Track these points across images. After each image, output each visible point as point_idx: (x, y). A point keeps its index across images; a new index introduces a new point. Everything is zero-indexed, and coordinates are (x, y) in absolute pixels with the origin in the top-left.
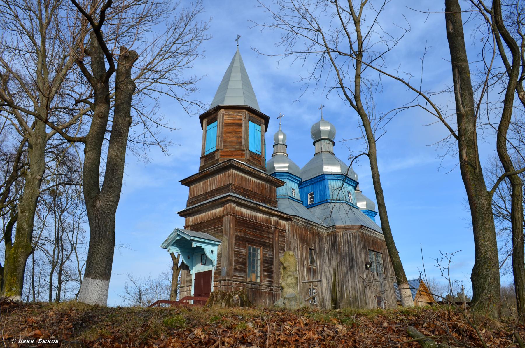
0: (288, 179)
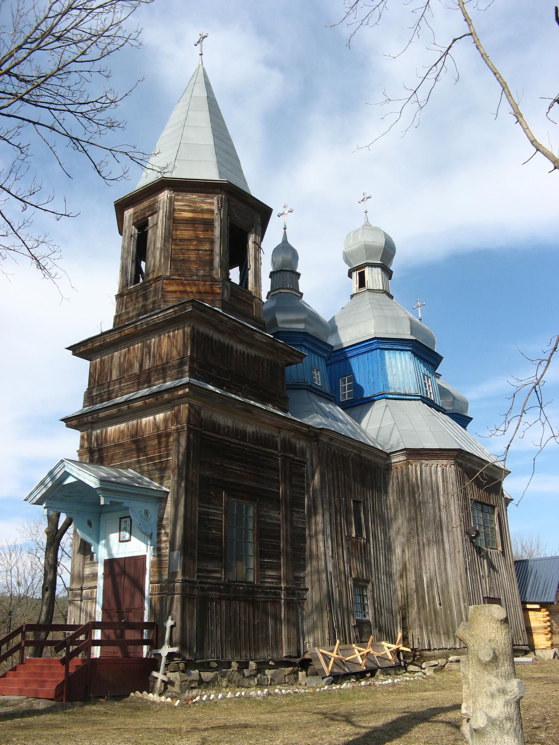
0: (306, 347)
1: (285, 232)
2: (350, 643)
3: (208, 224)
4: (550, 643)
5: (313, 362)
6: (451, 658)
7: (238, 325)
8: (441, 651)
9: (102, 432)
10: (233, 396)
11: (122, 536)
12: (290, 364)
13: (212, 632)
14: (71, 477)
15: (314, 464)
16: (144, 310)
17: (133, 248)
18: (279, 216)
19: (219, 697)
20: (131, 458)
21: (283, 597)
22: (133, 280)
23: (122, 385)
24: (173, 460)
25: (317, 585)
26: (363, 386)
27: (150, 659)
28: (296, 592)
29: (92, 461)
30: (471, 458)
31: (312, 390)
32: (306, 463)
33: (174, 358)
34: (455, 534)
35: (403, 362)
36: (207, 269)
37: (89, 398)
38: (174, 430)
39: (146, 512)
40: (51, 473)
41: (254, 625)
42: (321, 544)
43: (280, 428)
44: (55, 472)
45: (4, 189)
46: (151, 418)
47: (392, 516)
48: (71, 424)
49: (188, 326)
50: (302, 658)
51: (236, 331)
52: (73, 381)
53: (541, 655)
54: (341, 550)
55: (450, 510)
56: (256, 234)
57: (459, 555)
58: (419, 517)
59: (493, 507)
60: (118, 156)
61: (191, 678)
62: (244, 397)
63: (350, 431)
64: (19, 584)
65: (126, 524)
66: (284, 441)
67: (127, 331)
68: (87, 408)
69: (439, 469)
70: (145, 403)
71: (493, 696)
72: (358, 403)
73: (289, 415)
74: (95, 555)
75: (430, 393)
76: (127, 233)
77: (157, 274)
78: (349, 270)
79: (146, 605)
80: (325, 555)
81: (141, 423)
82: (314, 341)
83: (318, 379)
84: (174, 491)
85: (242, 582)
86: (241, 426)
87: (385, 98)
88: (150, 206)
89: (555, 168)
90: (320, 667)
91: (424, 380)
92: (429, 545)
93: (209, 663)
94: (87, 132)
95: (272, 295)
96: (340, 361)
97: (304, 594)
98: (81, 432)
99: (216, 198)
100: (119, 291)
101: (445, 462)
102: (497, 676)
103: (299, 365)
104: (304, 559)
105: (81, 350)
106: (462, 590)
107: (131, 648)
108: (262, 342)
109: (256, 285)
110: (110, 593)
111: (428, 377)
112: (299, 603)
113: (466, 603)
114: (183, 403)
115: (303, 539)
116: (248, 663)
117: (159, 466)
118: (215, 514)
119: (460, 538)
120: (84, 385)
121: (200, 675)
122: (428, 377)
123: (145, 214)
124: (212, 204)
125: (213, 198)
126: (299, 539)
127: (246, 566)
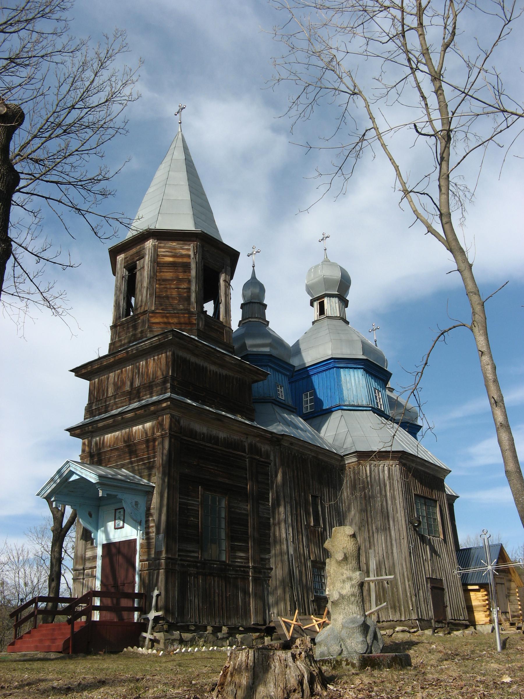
0: (271, 367)
1: (254, 270)
2: (309, 614)
3: (186, 267)
4: (489, 619)
5: (277, 379)
6: (398, 629)
7: (210, 349)
8: (389, 623)
9: (100, 440)
10: (208, 408)
11: (116, 524)
12: (257, 381)
13: (191, 601)
14: (75, 475)
15: (277, 464)
16: (134, 338)
17: (124, 287)
19: (195, 650)
20: (125, 460)
21: (250, 574)
22: (125, 313)
23: (117, 400)
24: (158, 460)
25: (280, 565)
26: (322, 399)
27: (141, 623)
28: (263, 571)
29: (92, 463)
30: (414, 458)
31: (277, 403)
32: (270, 464)
33: (158, 377)
34: (400, 524)
35: (357, 378)
36: (186, 303)
37: (89, 411)
38: (158, 436)
39: (137, 503)
40: (59, 472)
41: (226, 597)
42: (283, 531)
43: (247, 434)
44: (62, 471)
45: (23, 247)
46: (140, 427)
47: (346, 509)
48: (74, 433)
49: (170, 351)
50: (267, 625)
51: (209, 355)
52: (74, 399)
53: (481, 630)
54: (301, 536)
55: (395, 504)
56: (226, 274)
57: (404, 542)
58: (369, 508)
59: (436, 501)
60: (110, 221)
61: (173, 637)
62: (216, 409)
63: (309, 437)
64: (26, 584)
65: (120, 514)
66: (250, 445)
67: (120, 355)
68: (88, 420)
69: (386, 468)
70: (136, 414)
71: (344, 581)
72: (318, 414)
73: (255, 424)
74: (95, 540)
75: (381, 405)
76: (119, 274)
77: (144, 308)
78: (311, 300)
79: (137, 579)
80: (287, 540)
81: (132, 431)
82: (280, 360)
83: (282, 394)
84: (158, 486)
85: (216, 561)
86: (214, 432)
87: (318, 174)
88: (137, 252)
89: (428, 232)
90: (282, 633)
91: (375, 393)
92: (377, 532)
93: (188, 626)
94: (86, 202)
95: (243, 324)
96: (303, 379)
97: (269, 573)
98: (83, 439)
99: (192, 245)
100: (113, 322)
101: (391, 462)
102: (347, 570)
103: (266, 382)
104: (269, 544)
105: (80, 372)
106: (407, 571)
107: (125, 614)
108: (232, 363)
109: (226, 316)
110: (108, 570)
111: (379, 391)
112: (265, 581)
113: (410, 582)
114: (166, 414)
115: (268, 526)
116: (221, 627)
117: (147, 465)
118: (193, 505)
119: (404, 526)
120: (85, 401)
121: (181, 635)
122: (379, 391)
123: (133, 259)
124: (189, 250)
125: (190, 245)
126: (265, 528)
127: (219, 548)
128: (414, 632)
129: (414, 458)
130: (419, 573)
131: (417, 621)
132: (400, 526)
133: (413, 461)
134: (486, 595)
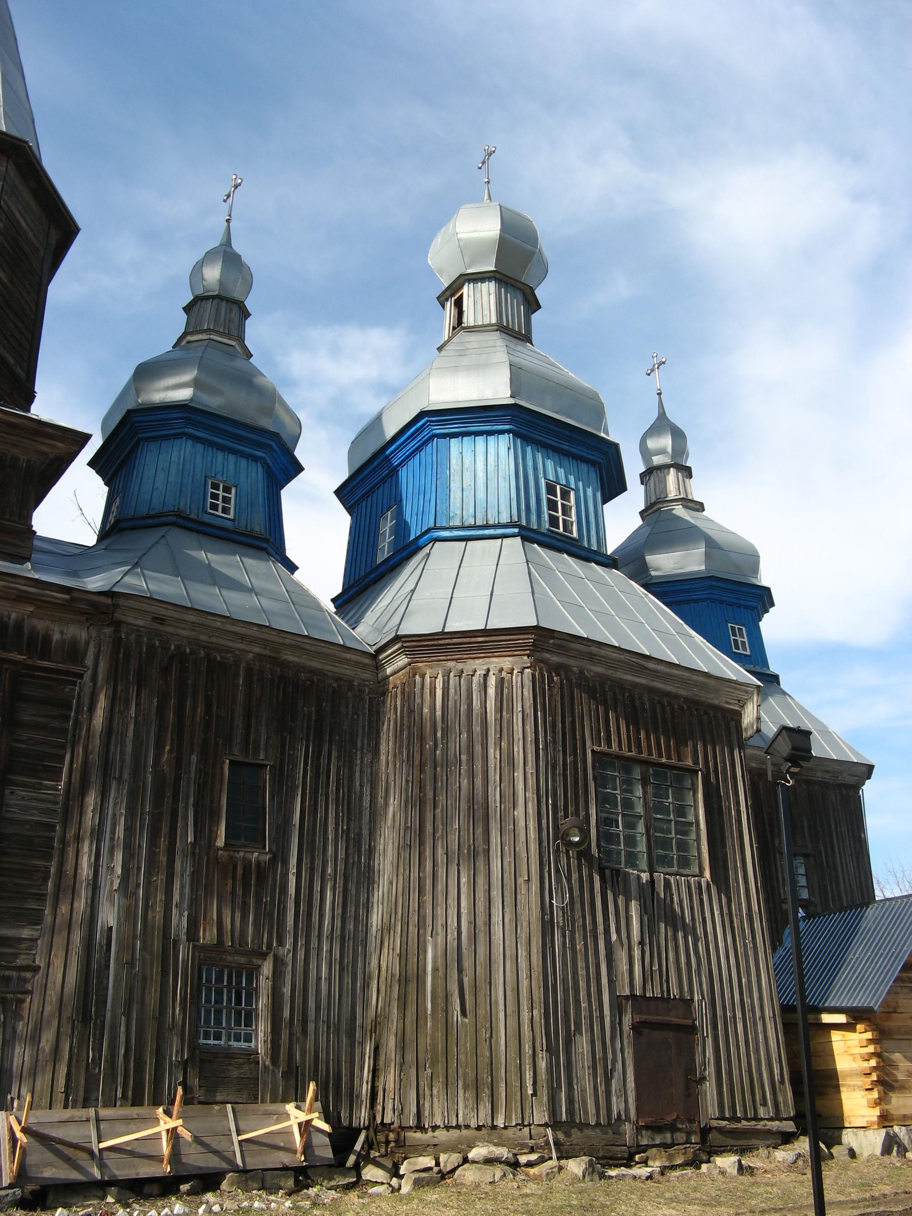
1: (660, 398)
4: (877, 1112)
8: (455, 1133)
18: (649, 375)
32: (80, 676)
97: (26, 980)
128: (530, 1164)
129: (594, 649)
130: (582, 984)
131: (549, 1131)
132: (521, 847)
133: (591, 657)
134: (870, 1041)
